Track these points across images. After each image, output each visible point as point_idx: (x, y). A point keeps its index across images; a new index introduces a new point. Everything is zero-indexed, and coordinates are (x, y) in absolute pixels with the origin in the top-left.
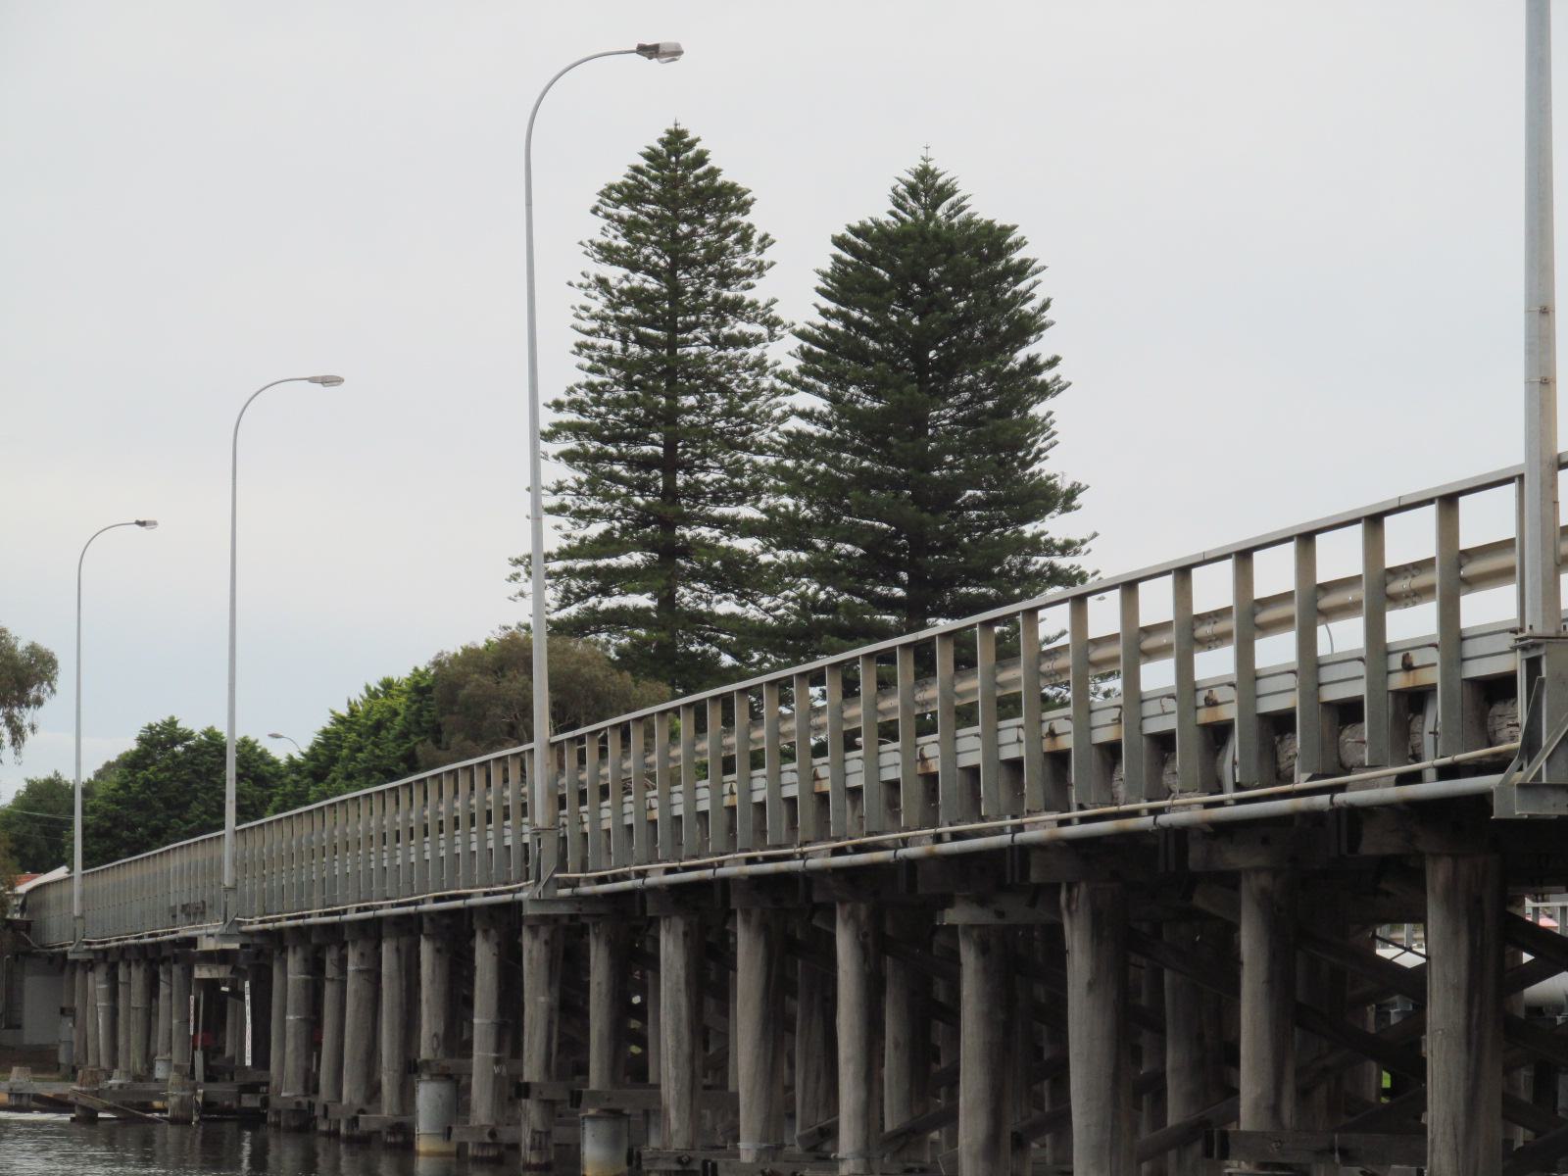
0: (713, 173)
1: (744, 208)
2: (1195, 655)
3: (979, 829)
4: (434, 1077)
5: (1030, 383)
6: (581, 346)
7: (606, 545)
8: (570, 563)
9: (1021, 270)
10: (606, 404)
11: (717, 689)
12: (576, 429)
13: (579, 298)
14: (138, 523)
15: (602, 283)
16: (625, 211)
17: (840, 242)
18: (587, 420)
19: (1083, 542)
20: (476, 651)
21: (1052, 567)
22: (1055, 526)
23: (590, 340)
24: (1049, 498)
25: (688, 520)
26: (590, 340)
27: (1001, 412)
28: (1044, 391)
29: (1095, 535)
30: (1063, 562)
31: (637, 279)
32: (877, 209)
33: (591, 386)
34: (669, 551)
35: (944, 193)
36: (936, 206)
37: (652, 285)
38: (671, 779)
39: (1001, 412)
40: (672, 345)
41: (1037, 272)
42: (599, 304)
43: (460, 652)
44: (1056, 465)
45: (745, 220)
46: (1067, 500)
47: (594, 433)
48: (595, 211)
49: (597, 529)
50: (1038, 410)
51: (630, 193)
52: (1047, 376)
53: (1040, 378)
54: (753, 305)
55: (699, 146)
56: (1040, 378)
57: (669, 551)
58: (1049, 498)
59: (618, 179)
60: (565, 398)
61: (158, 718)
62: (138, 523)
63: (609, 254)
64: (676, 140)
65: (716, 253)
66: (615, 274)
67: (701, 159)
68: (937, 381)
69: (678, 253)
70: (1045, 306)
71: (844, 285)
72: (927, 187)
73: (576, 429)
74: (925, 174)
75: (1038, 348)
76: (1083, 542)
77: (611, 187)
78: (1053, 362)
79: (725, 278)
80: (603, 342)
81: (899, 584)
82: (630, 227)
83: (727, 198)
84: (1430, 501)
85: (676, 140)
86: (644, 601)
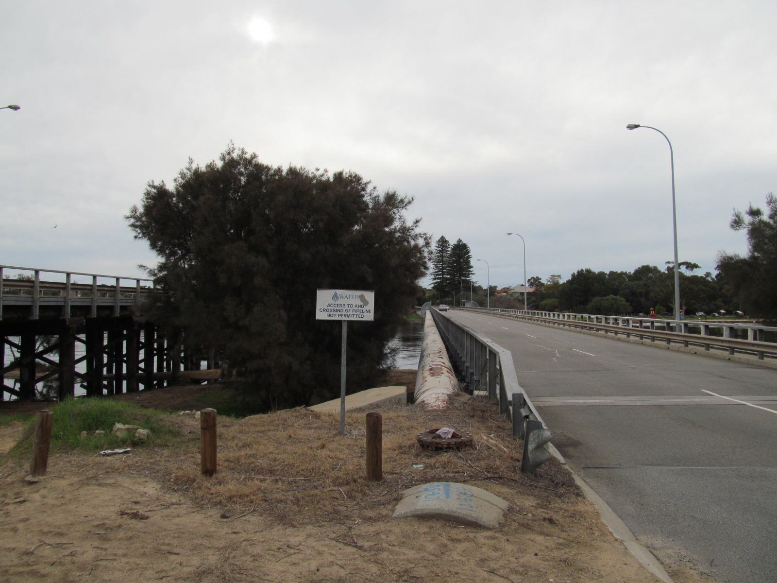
3: (679, 304)
4: (407, 390)
5: (469, 257)
11: (346, 340)
14: (10, 107)
22: (471, 269)
28: (470, 258)
34: (443, 272)
43: (285, 170)
46: (472, 267)
49: (437, 270)
57: (443, 272)
62: (10, 107)
63: (437, 247)
64: (442, 237)
66: (437, 248)
68: (461, 257)
72: (460, 241)
74: (459, 239)
75: (470, 254)
82: (439, 244)
83: (446, 242)
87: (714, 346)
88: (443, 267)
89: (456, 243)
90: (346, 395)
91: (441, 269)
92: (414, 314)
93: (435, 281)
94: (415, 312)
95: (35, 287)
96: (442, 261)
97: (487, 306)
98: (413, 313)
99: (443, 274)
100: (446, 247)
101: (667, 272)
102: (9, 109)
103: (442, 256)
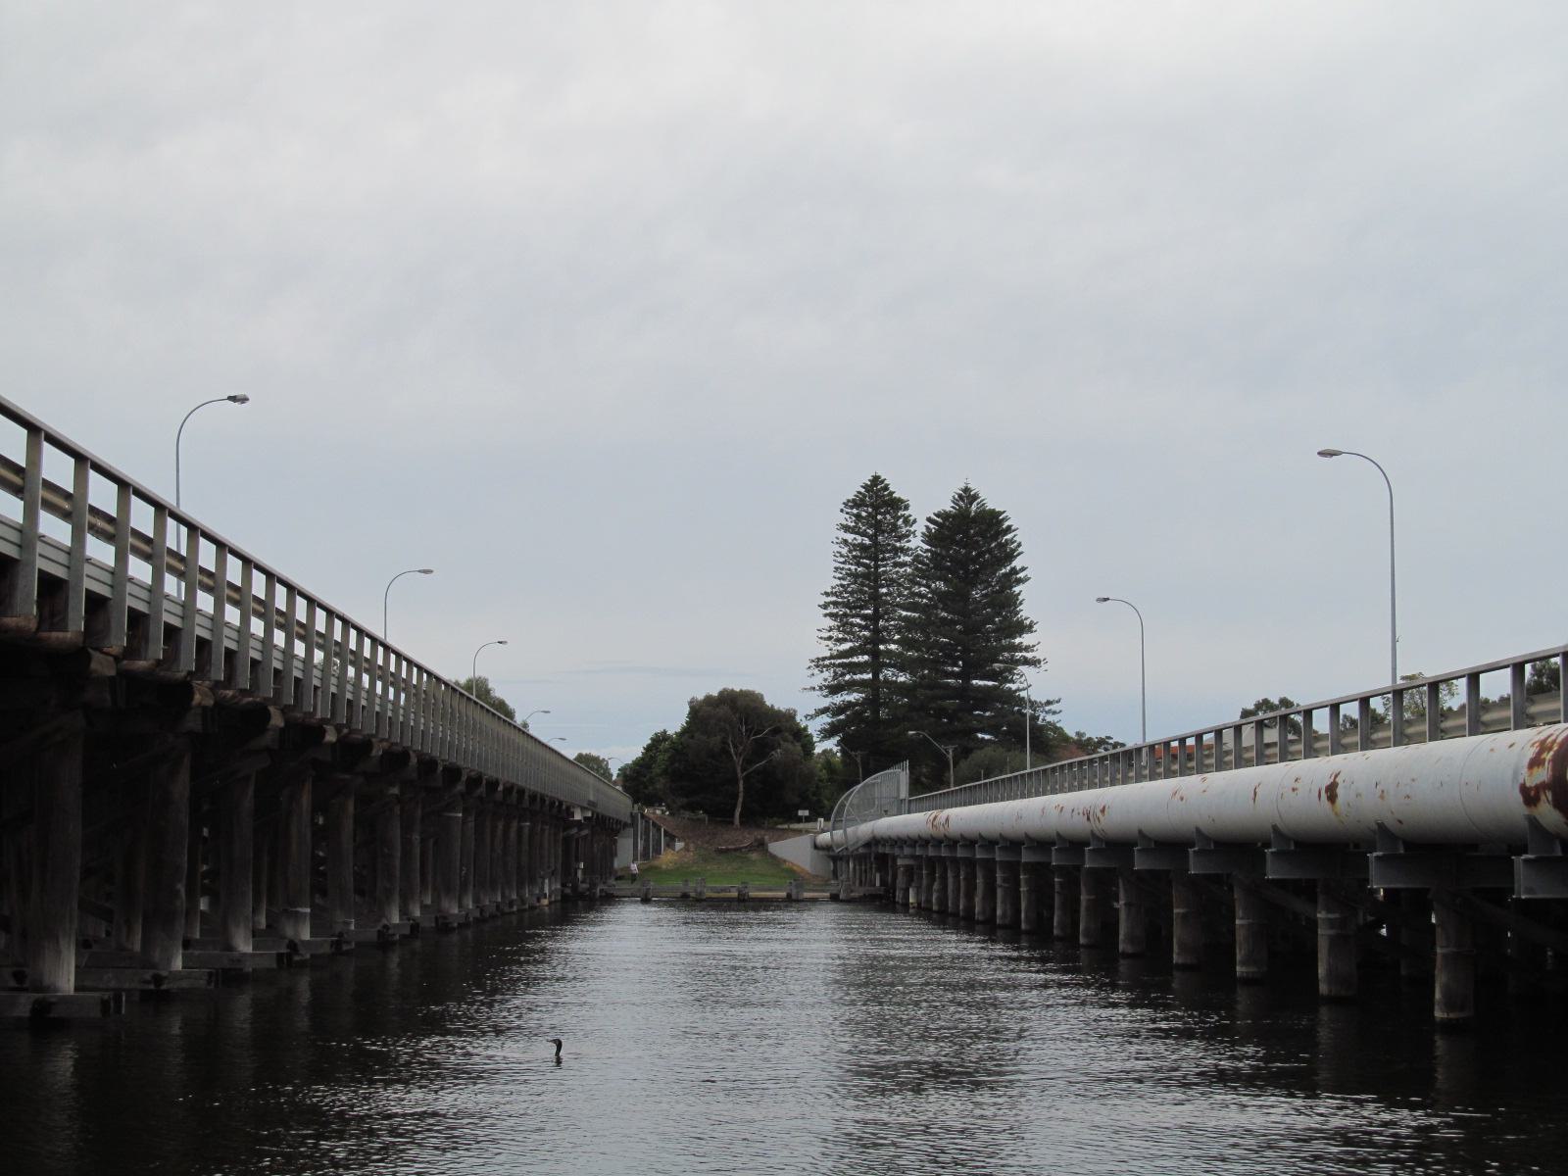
0: (892, 493)
1: (906, 508)
2: (27, 1015)
5: (1013, 578)
6: (836, 568)
8: (833, 661)
9: (1009, 529)
10: (850, 592)
12: (835, 604)
13: (837, 548)
14: (233, 399)
15: (845, 542)
16: (855, 511)
17: (929, 520)
18: (840, 600)
19: (1034, 646)
20: (763, 703)
21: (1024, 657)
22: (1025, 639)
23: (842, 566)
24: (1023, 628)
25: (884, 641)
26: (842, 566)
27: (1001, 591)
29: (1039, 643)
30: (1029, 655)
31: (859, 539)
32: (947, 506)
33: (842, 586)
34: (876, 654)
35: (975, 497)
36: (971, 504)
37: (867, 541)
38: (253, 932)
39: (1001, 591)
40: (877, 567)
41: (1014, 531)
44: (1026, 612)
45: (907, 513)
46: (1029, 628)
47: (846, 605)
48: (842, 511)
49: (846, 646)
50: (1017, 589)
51: (856, 503)
52: (1021, 575)
53: (1018, 576)
54: (909, 549)
55: (886, 482)
56: (1018, 576)
57: (876, 654)
58: (1023, 628)
59: (851, 497)
60: (829, 590)
61: (659, 730)
62: (233, 399)
63: (846, 529)
64: (876, 480)
65: (895, 527)
66: (850, 537)
67: (886, 488)
68: (971, 580)
69: (878, 527)
70: (1019, 545)
71: (929, 538)
72: (967, 496)
73: (835, 604)
74: (967, 490)
75: (1017, 563)
76: (1034, 646)
77: (849, 501)
78: (1023, 569)
79: (900, 538)
80: (847, 567)
81: (958, 666)
82: (858, 516)
83: (896, 504)
84: (1356, 700)
85: (876, 480)
88: (876, 631)
92: (754, 856)
96: (876, 598)
98: (751, 848)
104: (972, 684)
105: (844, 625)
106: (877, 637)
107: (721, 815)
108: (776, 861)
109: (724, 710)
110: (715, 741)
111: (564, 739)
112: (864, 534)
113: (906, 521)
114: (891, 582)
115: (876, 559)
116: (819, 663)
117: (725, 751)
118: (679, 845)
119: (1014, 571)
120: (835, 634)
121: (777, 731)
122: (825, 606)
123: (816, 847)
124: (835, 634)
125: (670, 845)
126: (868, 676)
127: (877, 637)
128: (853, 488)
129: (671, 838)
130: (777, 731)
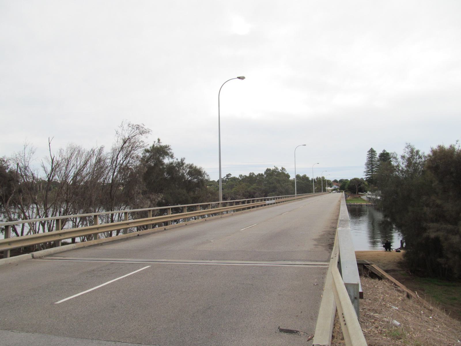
7: (369, 170)
14: (239, 78)
25: (373, 169)
32: (382, 152)
34: (372, 171)
35: (385, 151)
37: (371, 156)
42: (368, 158)
51: (369, 151)
57: (372, 171)
62: (239, 78)
63: (368, 155)
64: (372, 148)
66: (368, 156)
71: (379, 156)
72: (384, 151)
74: (384, 150)
82: (369, 153)
83: (374, 151)
85: (372, 148)
86: (371, 173)
87: (55, 213)
88: (372, 168)
89: (382, 152)
90: (28, 223)
91: (371, 169)
92: (359, 198)
93: (367, 176)
94: (360, 197)
95: (324, 193)
96: (372, 164)
97: (313, 192)
98: (359, 197)
99: (372, 172)
100: (374, 154)
101: (403, 165)
102: (238, 79)
103: (372, 161)
104: (405, 247)
105: (368, 167)
106: (372, 168)
107: (355, 193)
108: (362, 199)
109: (355, 181)
110: (354, 184)
111: (305, 145)
112: (370, 155)
113: (376, 153)
114: (374, 161)
115: (372, 158)
116: (365, 172)
117: (355, 185)
118: (350, 197)
119: (391, 160)
120: (367, 168)
121: (361, 183)
122: (365, 165)
123: (367, 197)
124: (367, 168)
125: (349, 197)
126: (371, 173)
127: (372, 168)
128: (369, 149)
129: (349, 196)
130: (361, 183)
